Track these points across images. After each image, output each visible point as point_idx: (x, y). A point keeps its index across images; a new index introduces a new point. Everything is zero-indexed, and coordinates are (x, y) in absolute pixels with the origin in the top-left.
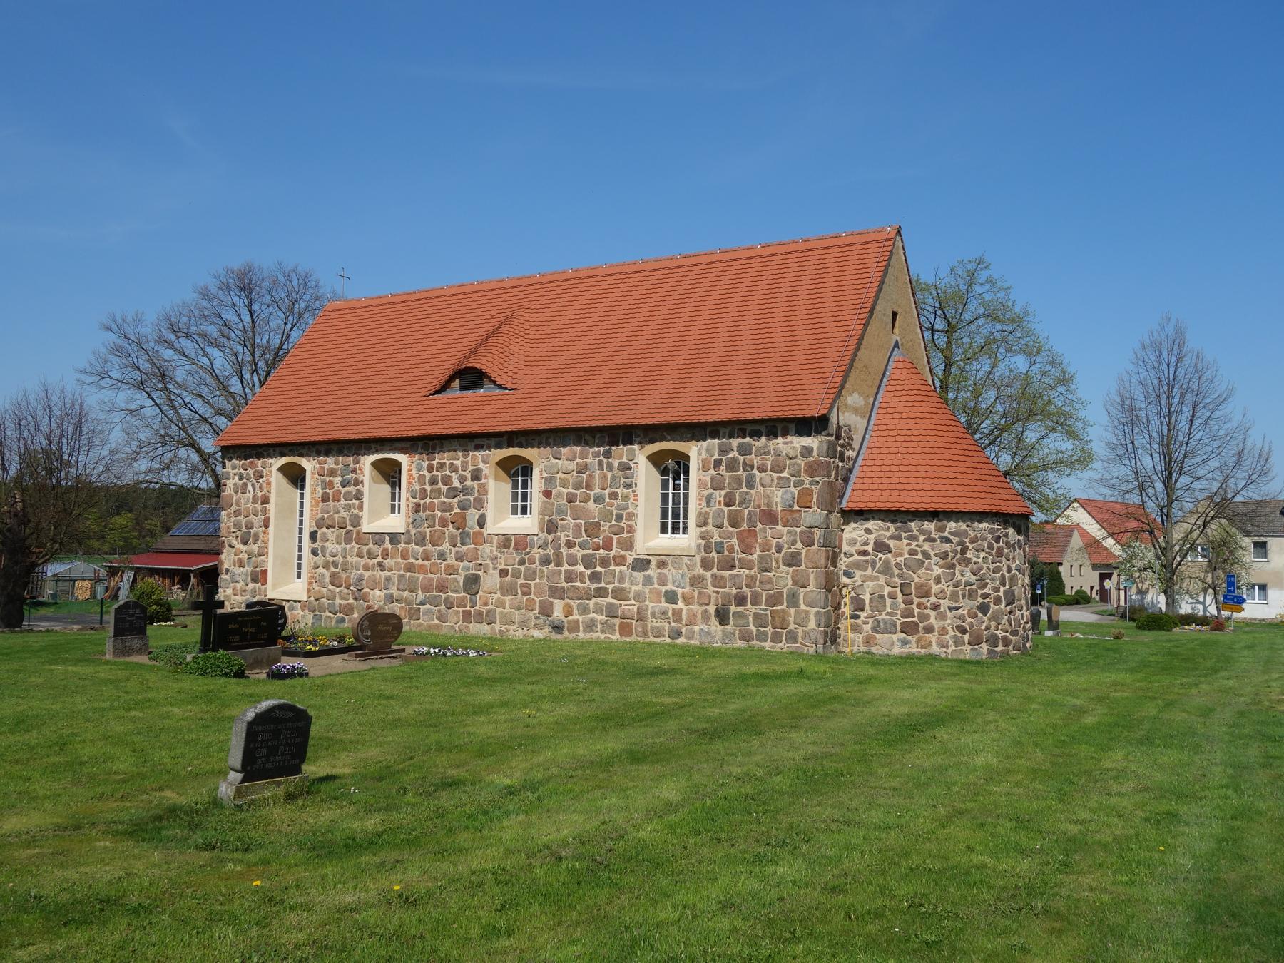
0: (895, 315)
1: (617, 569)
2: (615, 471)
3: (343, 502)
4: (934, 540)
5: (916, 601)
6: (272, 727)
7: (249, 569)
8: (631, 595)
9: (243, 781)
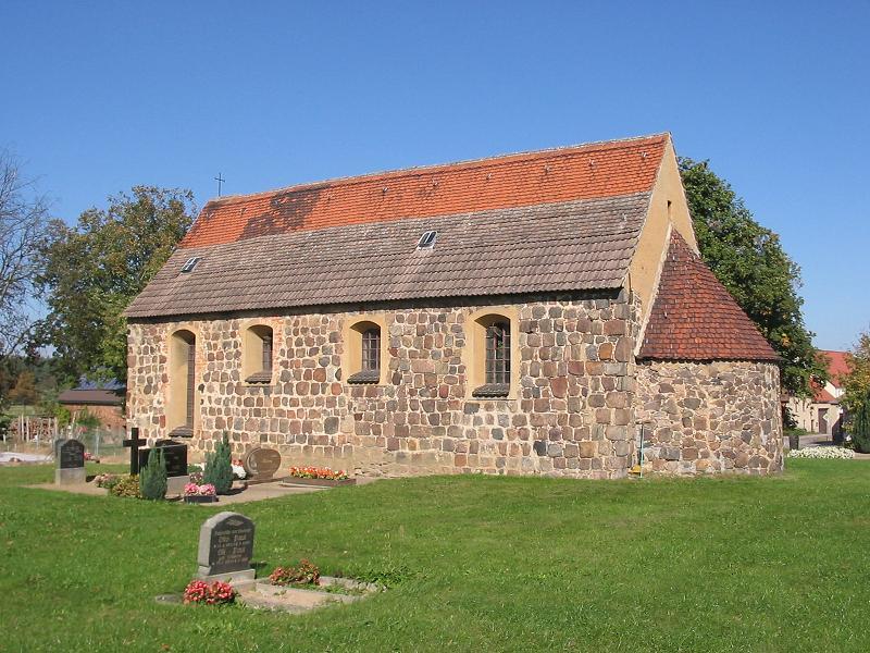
0: (669, 203)
1: (452, 412)
2: (449, 332)
3: (225, 360)
4: (708, 384)
5: (695, 432)
6: (228, 532)
7: (151, 414)
8: (464, 434)
9: (211, 573)
